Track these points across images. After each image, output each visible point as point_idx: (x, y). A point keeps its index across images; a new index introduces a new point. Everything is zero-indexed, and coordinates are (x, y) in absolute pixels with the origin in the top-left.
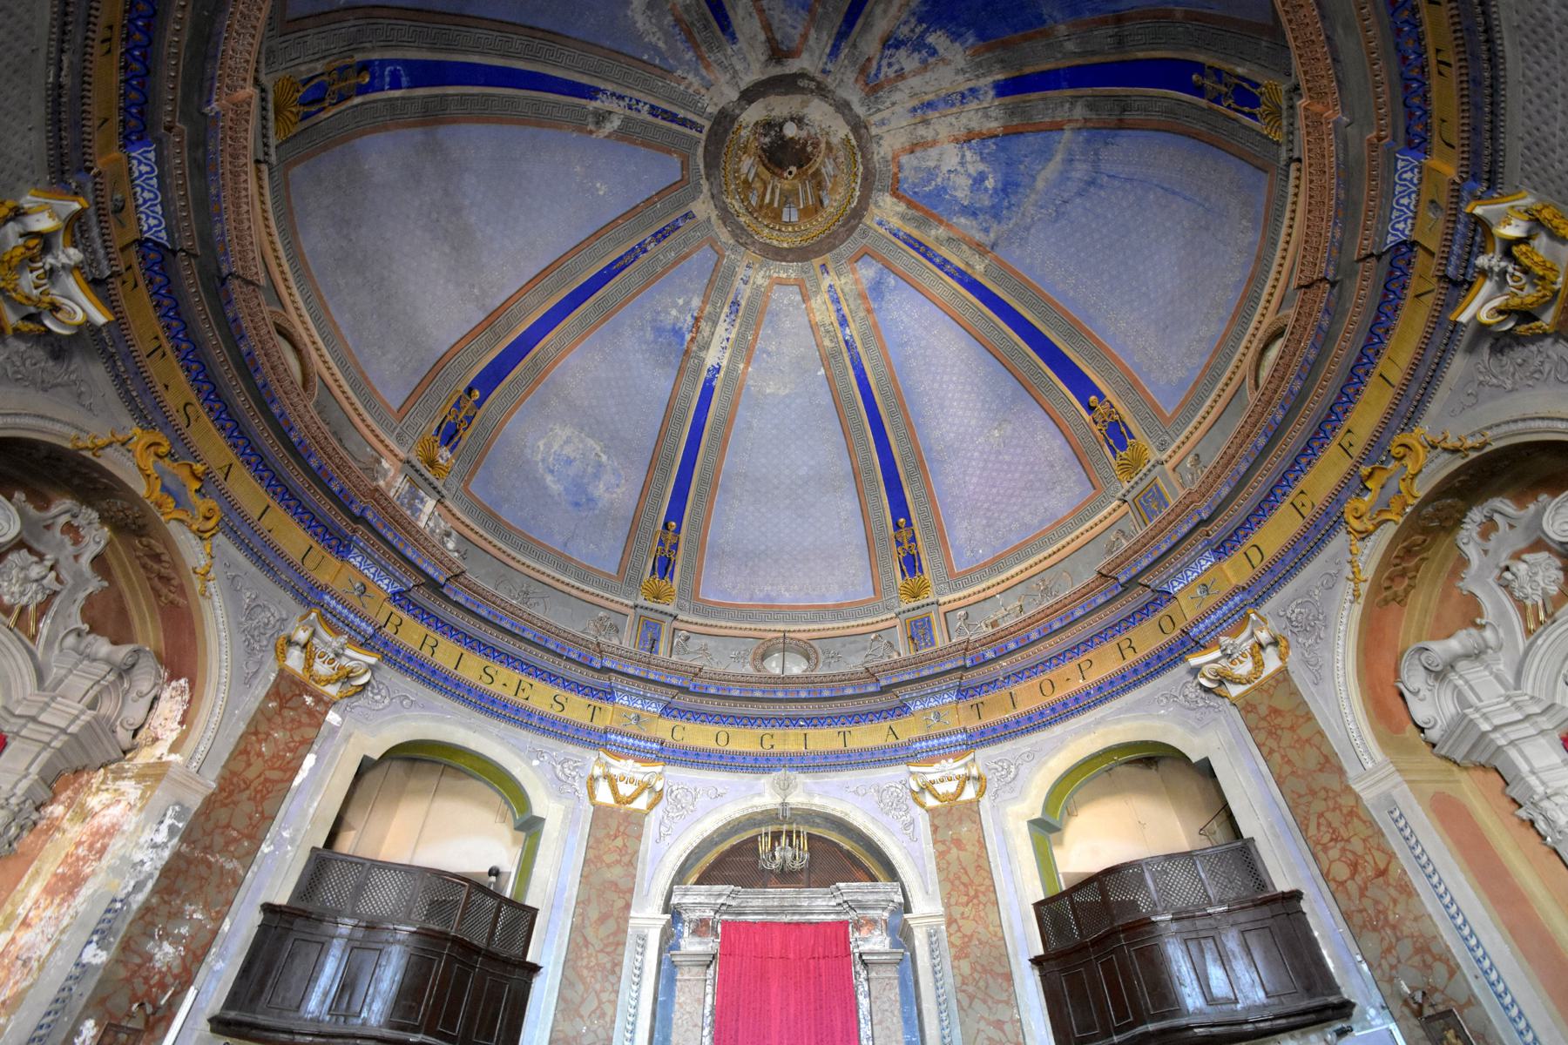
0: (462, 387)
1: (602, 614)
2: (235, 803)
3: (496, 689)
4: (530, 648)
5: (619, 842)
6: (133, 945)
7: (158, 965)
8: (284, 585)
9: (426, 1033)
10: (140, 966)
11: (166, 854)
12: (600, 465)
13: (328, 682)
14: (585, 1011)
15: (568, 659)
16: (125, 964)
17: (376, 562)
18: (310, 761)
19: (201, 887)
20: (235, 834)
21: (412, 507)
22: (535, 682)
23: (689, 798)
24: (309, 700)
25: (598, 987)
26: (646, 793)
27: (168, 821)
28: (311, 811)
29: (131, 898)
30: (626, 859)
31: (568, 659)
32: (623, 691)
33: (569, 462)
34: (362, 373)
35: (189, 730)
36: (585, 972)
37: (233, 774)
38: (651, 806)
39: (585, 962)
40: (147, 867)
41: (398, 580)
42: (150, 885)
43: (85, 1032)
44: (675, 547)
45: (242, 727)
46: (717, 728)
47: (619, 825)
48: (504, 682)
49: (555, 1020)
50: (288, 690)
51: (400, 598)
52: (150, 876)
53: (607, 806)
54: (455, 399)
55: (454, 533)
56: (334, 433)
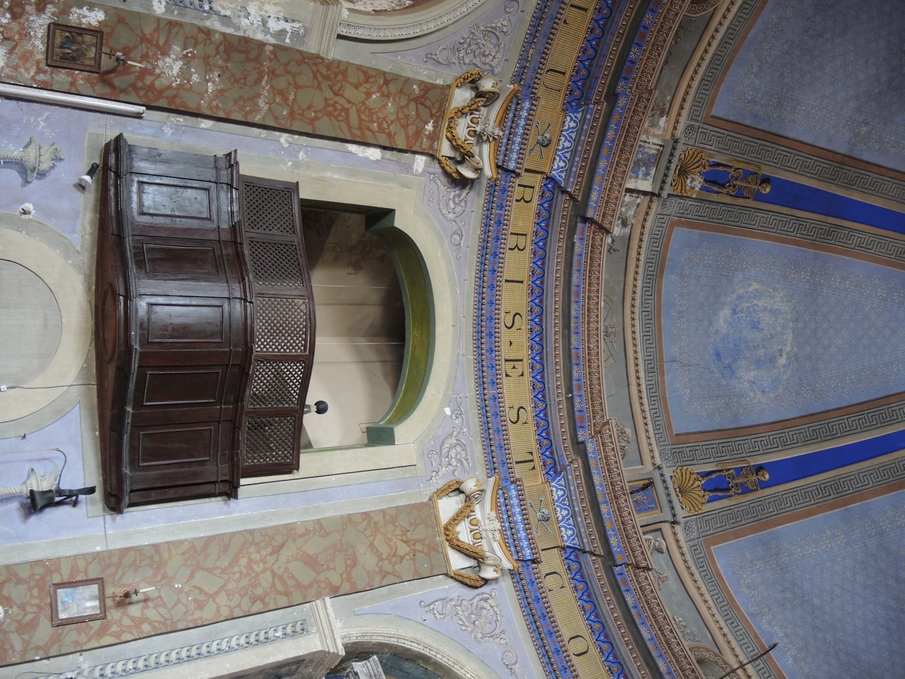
0: (766, 171)
1: (629, 431)
2: (319, 87)
3: (505, 335)
4: (560, 352)
5: (403, 549)
6: (175, 30)
7: (160, 63)
8: (524, 58)
9: (143, 356)
10: (157, 46)
11: (260, 37)
12: (773, 360)
13: (452, 139)
14: (201, 578)
15: (571, 401)
16: (157, 29)
17: (577, 142)
18: (374, 154)
19: (237, 81)
20: (291, 97)
21: (637, 164)
22: (527, 378)
23: (488, 629)
24: (430, 127)
25: (231, 586)
26: (471, 563)
27: (288, 26)
28: (329, 174)
29: (215, 17)
30: (387, 567)
31: (571, 401)
32: (567, 485)
33: (755, 326)
34: (731, 62)
35: (372, 15)
36: (243, 561)
37: (344, 73)
38: (458, 578)
39: (256, 557)
40: (245, 22)
41: (569, 172)
42: (230, 31)
43: (93, 14)
44: (746, 491)
45: (387, 69)
46: (585, 631)
47: (422, 541)
48: (515, 342)
49: (181, 542)
50: (431, 100)
51: (552, 185)
52: (238, 28)
53: (436, 517)
54: (751, 168)
55: (627, 230)
56: (670, 53)
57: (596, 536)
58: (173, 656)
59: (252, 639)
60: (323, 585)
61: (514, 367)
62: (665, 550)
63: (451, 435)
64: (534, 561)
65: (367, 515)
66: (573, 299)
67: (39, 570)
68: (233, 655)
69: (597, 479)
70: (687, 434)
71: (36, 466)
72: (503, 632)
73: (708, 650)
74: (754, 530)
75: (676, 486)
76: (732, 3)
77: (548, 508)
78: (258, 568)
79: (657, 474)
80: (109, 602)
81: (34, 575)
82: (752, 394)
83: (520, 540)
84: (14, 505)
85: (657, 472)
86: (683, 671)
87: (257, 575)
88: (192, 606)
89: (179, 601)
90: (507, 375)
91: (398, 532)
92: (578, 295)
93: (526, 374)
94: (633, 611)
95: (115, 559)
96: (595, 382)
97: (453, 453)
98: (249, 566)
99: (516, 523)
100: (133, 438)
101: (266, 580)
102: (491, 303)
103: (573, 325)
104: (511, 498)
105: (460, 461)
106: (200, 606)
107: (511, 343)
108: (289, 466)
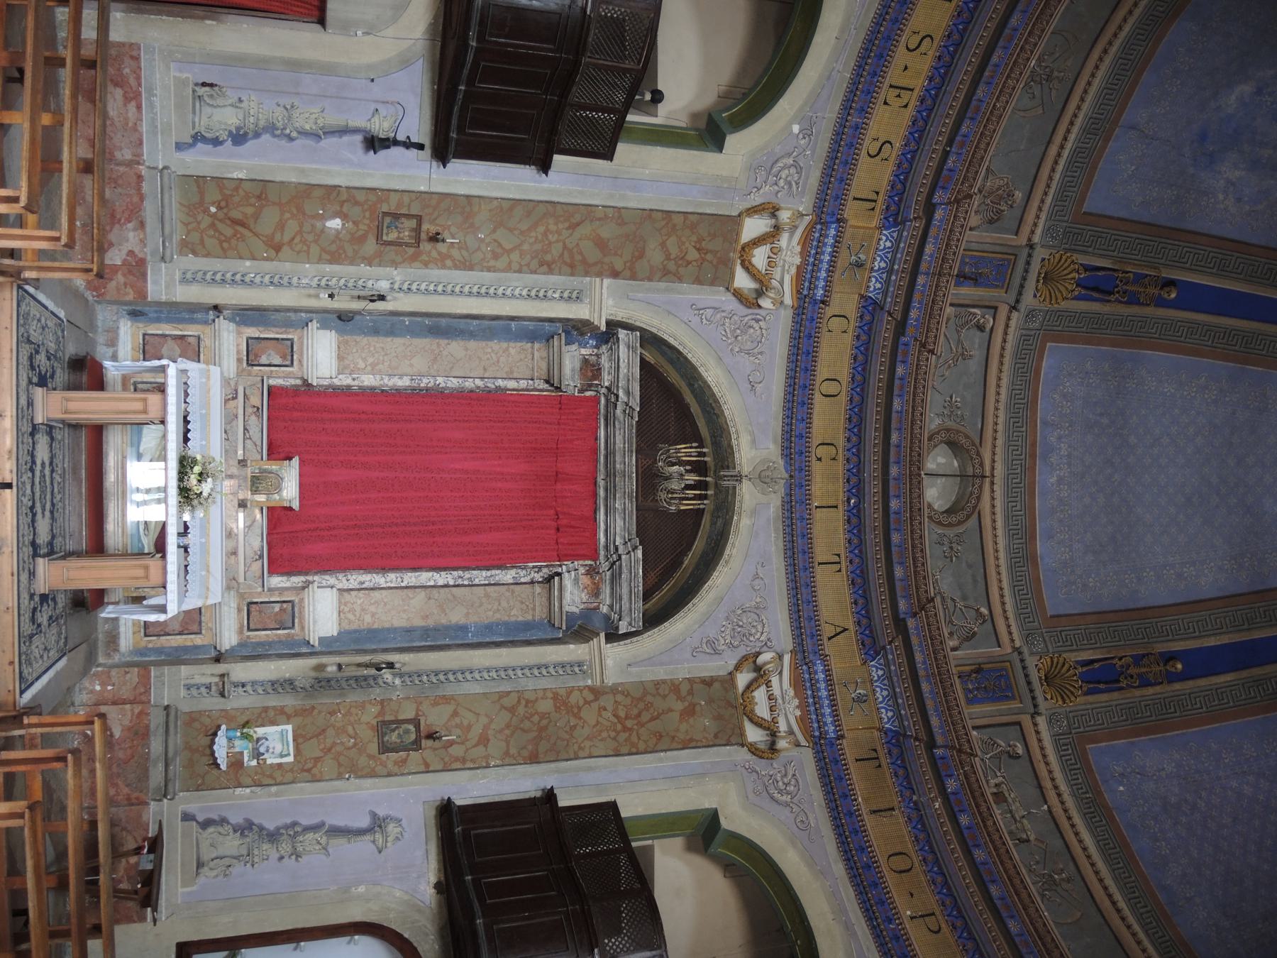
1: (1019, 195)
3: (901, 56)
5: (693, 255)
15: (946, 154)
22: (910, 112)
23: (749, 345)
30: (671, 266)
31: (946, 154)
32: (898, 240)
36: (541, 229)
38: (738, 294)
39: (552, 227)
47: (714, 252)
53: (738, 234)
57: (901, 300)
58: (466, 289)
59: (533, 293)
60: (606, 267)
61: (899, 96)
62: (988, 329)
63: (789, 155)
64: (823, 302)
65: (668, 213)
66: (1001, 43)
67: (372, 198)
68: (514, 302)
69: (929, 249)
70: (1100, 216)
71: (380, 107)
72: (761, 353)
73: (967, 437)
74: (1114, 344)
75: (1043, 271)
76: (1136, 5)
77: (867, 254)
78: (552, 238)
79: (1026, 251)
80: (423, 236)
81: (368, 200)
82: (1221, 197)
83: (817, 278)
84: (359, 138)
85: (1026, 251)
86: (911, 450)
87: (550, 243)
88: (489, 256)
89: (479, 249)
90: (885, 103)
91: (694, 238)
92: (1011, 39)
93: (911, 106)
94: (897, 382)
95: (433, 202)
96: (982, 146)
97: (784, 174)
98: (545, 234)
99: (821, 261)
100: (463, 108)
101: (556, 250)
102: (896, 21)
103: (986, 73)
104: (826, 236)
105: (790, 184)
106: (496, 256)
107: (906, 68)
108: (607, 154)
